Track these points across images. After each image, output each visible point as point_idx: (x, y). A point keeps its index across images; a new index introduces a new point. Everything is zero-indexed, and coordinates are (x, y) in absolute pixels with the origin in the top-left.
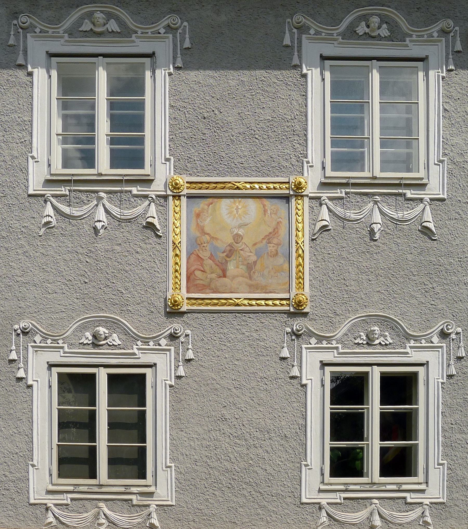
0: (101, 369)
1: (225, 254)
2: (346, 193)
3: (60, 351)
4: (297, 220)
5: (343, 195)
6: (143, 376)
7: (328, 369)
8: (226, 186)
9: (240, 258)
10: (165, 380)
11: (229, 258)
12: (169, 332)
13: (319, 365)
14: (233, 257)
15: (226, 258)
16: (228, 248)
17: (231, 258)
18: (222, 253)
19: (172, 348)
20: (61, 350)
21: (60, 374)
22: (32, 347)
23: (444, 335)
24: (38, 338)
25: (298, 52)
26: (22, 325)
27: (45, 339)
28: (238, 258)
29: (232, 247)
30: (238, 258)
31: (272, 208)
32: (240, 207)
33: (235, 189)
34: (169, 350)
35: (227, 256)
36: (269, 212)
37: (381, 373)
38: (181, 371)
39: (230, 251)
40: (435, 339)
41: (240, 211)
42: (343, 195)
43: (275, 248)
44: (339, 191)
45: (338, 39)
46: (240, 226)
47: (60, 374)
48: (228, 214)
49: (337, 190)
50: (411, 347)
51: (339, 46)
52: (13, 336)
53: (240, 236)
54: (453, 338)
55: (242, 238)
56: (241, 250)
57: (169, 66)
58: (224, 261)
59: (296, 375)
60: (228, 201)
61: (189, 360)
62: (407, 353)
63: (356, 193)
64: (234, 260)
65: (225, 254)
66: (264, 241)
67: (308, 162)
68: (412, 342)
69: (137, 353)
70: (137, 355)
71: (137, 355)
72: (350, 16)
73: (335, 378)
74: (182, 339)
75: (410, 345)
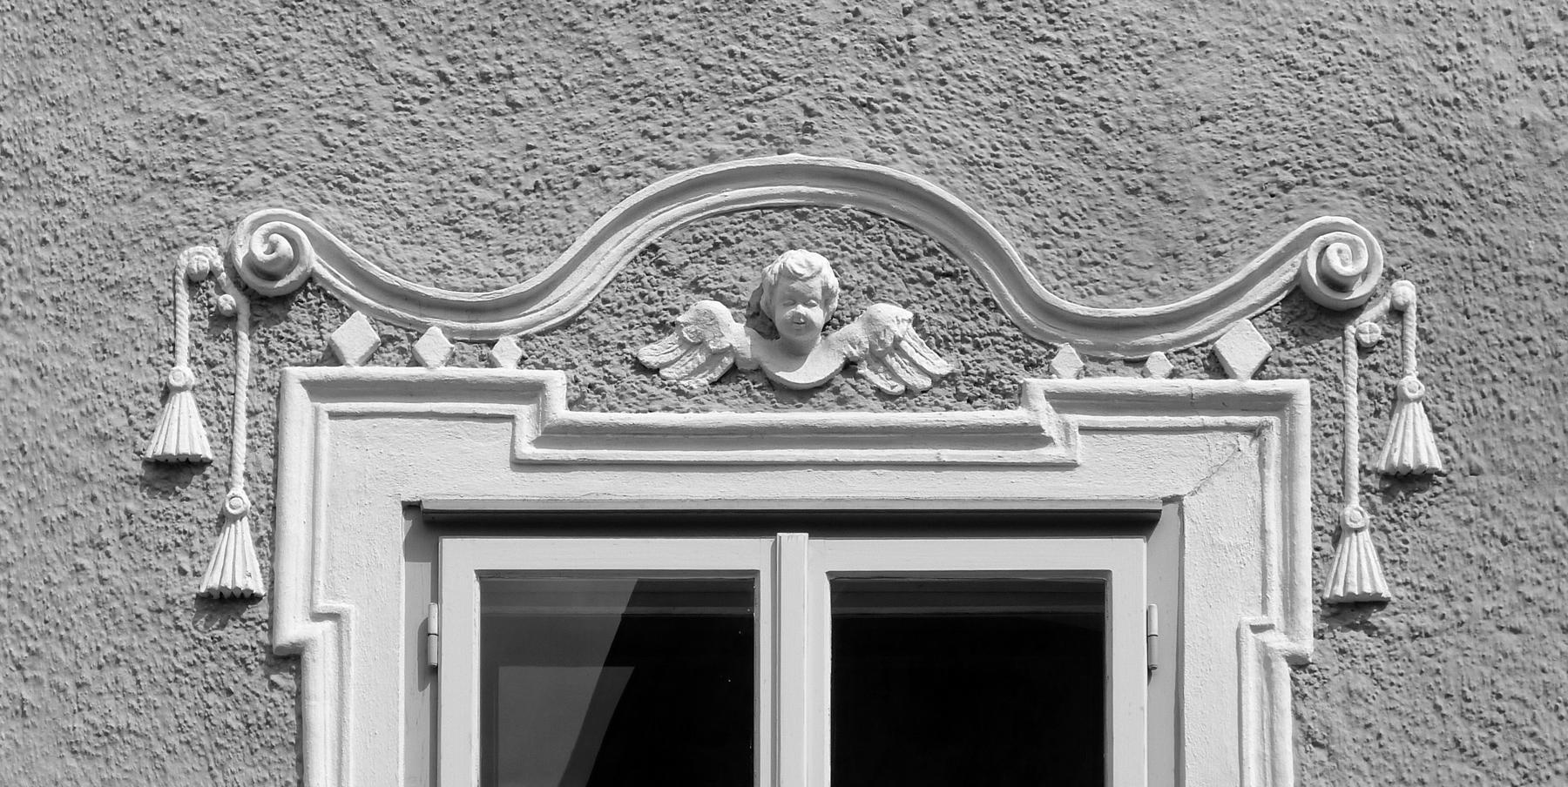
0: (795, 543)
3: (511, 418)
6: (1092, 591)
7: (465, 558)
10: (1257, 629)
12: (1283, 276)
13: (399, 527)
19: (1300, 388)
20: (524, 411)
21: (493, 583)
22: (317, 389)
23: (1313, 312)
24: (355, 335)
26: (253, 246)
27: (396, 340)
34: (1279, 403)
37: (845, 588)
38: (1362, 568)
40: (1245, 346)
47: (493, 583)
50: (1063, 401)
52: (184, 326)
54: (1366, 339)
59: (1368, 589)
61: (1404, 482)
62: (1031, 436)
68: (1067, 359)
69: (1051, 430)
70: (1048, 441)
71: (1048, 441)
73: (518, 626)
74: (1368, 326)
75: (1054, 384)
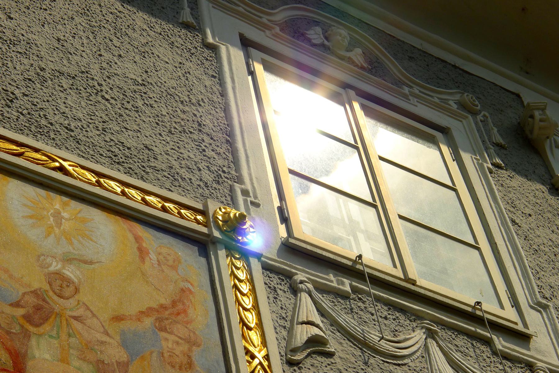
1: (21, 312)
2: (355, 290)
4: (242, 320)
5: (348, 288)
8: (27, 154)
9: (72, 340)
11: (37, 326)
14: (46, 327)
15: (22, 321)
16: (31, 300)
17: (41, 330)
18: (11, 305)
25: (192, 9)
28: (64, 336)
29: (44, 300)
30: (64, 336)
31: (164, 251)
32: (65, 215)
33: (54, 169)
35: (27, 318)
36: (153, 256)
39: (38, 308)
41: (66, 225)
42: (348, 288)
43: (185, 347)
44: (331, 277)
45: (273, 28)
46: (68, 260)
48: (31, 217)
49: (327, 274)
51: (273, 37)
53: (69, 281)
55: (77, 291)
56: (76, 318)
57: (483, 154)
58: (16, 329)
60: (31, 190)
63: (378, 299)
64: (51, 337)
65: (21, 312)
66: (148, 322)
67: (245, 193)
72: (288, 9)
